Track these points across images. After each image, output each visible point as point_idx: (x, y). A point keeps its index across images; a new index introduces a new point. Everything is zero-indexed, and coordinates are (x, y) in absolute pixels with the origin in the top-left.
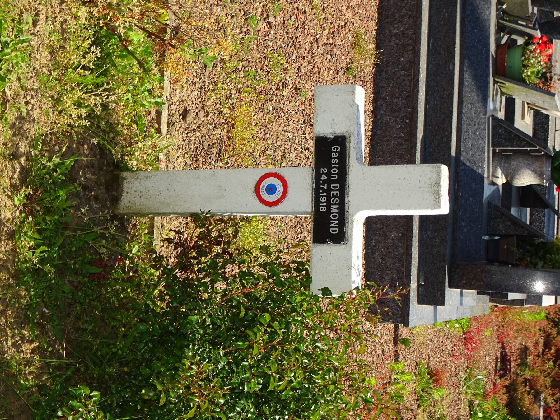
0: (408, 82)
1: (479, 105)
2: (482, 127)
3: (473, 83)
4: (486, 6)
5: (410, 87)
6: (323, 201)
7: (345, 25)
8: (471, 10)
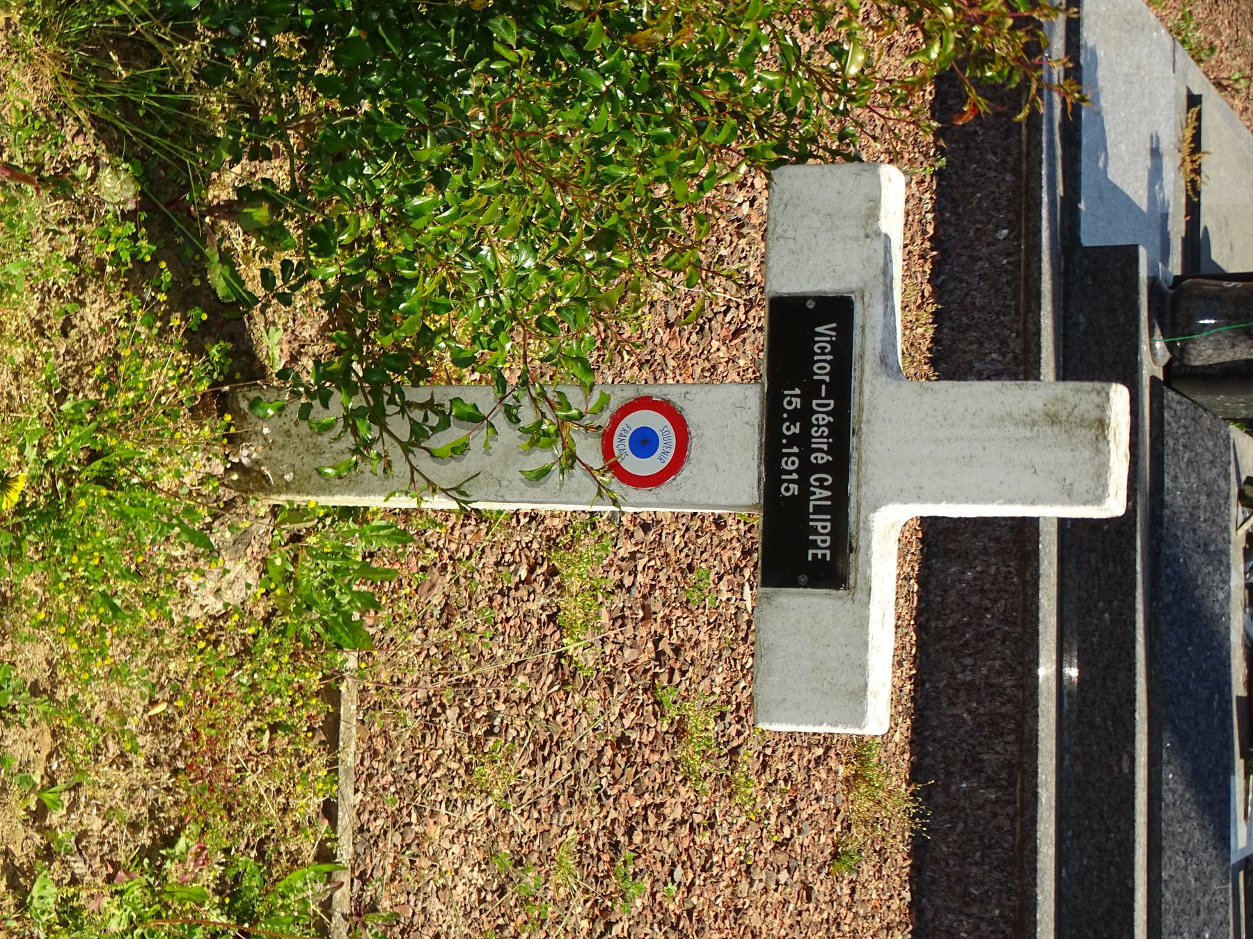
0: (1007, 823)
1: (1206, 856)
2: (1218, 917)
3: (1188, 796)
4: (1217, 578)
5: (1013, 835)
6: (790, 468)
7: (825, 753)
8: (1174, 592)
